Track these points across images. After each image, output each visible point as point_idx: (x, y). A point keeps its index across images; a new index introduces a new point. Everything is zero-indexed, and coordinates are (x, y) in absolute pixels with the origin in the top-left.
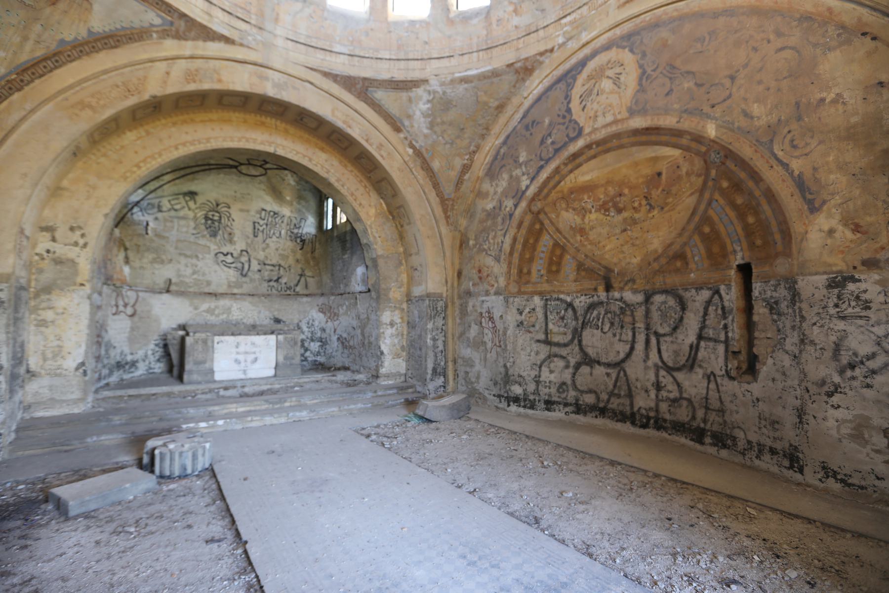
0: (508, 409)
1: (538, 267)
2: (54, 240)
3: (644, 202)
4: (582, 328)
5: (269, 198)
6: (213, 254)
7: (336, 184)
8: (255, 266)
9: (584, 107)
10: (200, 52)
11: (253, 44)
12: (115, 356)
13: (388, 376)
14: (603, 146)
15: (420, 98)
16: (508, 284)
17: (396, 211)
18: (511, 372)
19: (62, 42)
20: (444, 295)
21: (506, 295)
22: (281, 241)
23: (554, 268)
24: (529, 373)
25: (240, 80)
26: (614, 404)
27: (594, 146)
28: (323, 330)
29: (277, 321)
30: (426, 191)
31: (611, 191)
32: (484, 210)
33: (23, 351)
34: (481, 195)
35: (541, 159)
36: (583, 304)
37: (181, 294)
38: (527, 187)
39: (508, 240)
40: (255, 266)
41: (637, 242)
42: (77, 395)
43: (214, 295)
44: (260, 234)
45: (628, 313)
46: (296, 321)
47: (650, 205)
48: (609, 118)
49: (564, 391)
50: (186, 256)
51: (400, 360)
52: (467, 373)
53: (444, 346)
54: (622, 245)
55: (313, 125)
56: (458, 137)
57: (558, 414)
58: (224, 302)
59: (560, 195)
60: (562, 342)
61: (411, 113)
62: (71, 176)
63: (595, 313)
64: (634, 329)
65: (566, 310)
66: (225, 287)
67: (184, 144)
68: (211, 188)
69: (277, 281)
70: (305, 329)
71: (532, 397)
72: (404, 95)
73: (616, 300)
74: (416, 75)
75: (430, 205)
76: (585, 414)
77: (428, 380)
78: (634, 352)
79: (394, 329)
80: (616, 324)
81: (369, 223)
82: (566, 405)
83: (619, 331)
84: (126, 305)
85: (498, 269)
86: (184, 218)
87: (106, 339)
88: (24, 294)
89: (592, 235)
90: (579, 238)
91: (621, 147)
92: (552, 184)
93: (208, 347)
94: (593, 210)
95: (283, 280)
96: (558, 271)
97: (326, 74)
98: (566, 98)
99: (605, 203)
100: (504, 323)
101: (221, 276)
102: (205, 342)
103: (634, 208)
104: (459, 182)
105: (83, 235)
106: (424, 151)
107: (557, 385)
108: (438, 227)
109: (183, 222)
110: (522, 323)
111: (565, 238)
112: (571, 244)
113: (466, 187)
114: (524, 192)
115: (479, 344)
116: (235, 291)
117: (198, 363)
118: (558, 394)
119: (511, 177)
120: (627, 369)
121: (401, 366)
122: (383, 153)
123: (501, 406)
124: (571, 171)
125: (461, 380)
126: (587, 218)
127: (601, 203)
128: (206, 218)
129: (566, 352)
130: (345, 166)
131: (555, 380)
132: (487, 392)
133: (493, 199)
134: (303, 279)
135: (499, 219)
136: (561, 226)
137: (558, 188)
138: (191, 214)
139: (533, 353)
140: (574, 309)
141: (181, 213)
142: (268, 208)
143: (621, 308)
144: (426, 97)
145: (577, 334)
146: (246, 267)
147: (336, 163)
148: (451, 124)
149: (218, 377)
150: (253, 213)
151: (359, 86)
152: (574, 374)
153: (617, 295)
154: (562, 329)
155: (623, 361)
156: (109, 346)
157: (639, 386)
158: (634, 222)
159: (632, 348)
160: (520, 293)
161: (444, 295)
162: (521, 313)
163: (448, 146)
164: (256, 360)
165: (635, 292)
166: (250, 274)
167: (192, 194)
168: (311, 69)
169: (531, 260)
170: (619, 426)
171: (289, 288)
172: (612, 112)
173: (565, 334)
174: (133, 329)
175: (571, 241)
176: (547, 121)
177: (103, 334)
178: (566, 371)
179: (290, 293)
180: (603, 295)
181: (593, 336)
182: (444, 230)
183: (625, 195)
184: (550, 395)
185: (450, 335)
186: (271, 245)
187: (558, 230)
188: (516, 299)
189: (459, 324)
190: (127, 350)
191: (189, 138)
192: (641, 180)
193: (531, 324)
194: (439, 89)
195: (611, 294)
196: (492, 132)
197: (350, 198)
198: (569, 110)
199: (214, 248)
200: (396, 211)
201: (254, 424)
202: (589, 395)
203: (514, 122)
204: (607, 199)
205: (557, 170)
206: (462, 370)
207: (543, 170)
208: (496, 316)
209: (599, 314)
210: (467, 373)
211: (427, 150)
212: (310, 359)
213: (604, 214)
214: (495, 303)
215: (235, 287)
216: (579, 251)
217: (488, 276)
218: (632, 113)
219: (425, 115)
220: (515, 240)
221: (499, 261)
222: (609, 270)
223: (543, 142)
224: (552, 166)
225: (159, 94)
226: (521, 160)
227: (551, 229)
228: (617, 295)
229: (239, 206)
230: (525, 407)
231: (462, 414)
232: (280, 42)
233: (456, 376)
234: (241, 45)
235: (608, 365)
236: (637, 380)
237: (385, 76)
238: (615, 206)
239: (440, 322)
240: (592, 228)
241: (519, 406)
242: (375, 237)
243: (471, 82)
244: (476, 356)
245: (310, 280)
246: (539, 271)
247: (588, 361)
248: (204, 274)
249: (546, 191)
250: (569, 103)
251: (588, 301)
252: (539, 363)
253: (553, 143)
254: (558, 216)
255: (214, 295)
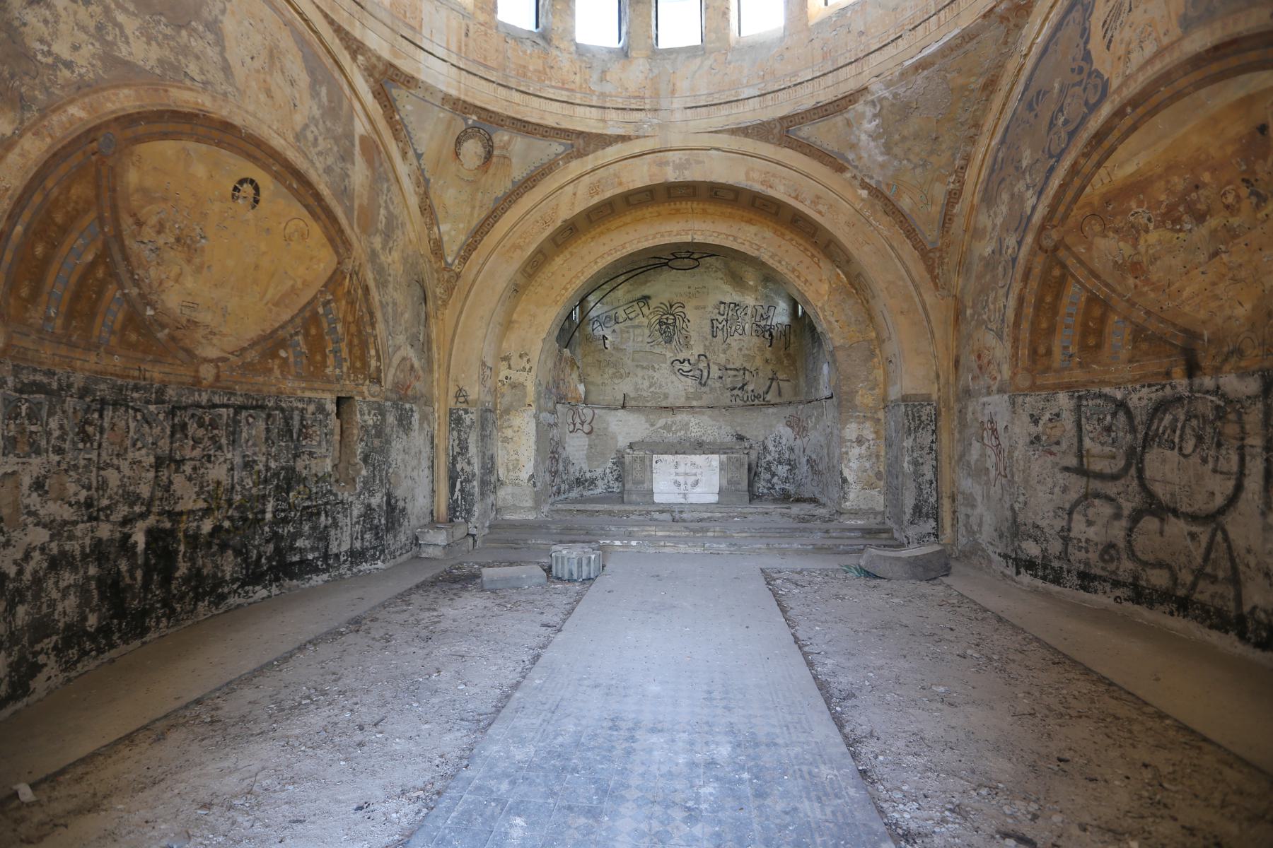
0: (1017, 579)
1: (1064, 342)
2: (510, 368)
3: (1244, 192)
4: (1144, 447)
5: (727, 288)
6: (669, 362)
7: (770, 262)
8: (715, 372)
9: (1110, 41)
10: (600, 162)
11: (649, 131)
12: (574, 472)
13: (856, 513)
14: (1144, 105)
15: (862, 115)
16: (1015, 374)
17: (856, 285)
18: (1021, 518)
19: (497, 198)
20: (935, 397)
21: (1013, 392)
22: (745, 338)
23: (1092, 341)
24: (1051, 524)
25: (639, 176)
26: (1205, 593)
27: (1129, 110)
28: (792, 449)
29: (740, 438)
30: (895, 244)
31: (1179, 183)
32: (982, 258)
33: (493, 463)
34: (977, 234)
35: (1051, 156)
36: (1144, 402)
37: (638, 409)
38: (1034, 208)
39: (1012, 302)
40: (715, 372)
41: (1243, 274)
42: (529, 503)
43: (672, 409)
44: (720, 333)
45: (1232, 417)
46: (761, 438)
47: (1258, 195)
48: (1150, 49)
49: (1112, 560)
50: (643, 368)
51: (875, 492)
52: (968, 516)
53: (935, 474)
54: (1214, 284)
55: (731, 196)
56: (931, 153)
57: (1102, 599)
58: (682, 417)
59: (1088, 211)
60: (1108, 471)
61: (853, 139)
62: (518, 309)
63: (1168, 418)
64: (1241, 449)
65: (1114, 415)
66: (683, 399)
67: (602, 257)
68: (663, 288)
69: (742, 388)
70: (772, 448)
71: (1056, 564)
72: (839, 120)
73: (1207, 392)
74: (852, 86)
75: (903, 264)
76: (1151, 605)
77: (905, 523)
78: (1243, 495)
79: (864, 447)
80: (1207, 440)
81: (820, 304)
82: (1116, 584)
83: (1212, 452)
84: (582, 423)
85: (1000, 350)
86: (638, 327)
87: (564, 455)
88: (489, 415)
89: (1156, 273)
90: (1131, 281)
91: (1177, 96)
92: (1070, 195)
93: (647, 468)
94: (1151, 226)
95: (750, 388)
96: (1098, 346)
97: (733, 132)
98: (1082, 37)
99: (1171, 208)
100: (1010, 438)
101: (678, 387)
102: (642, 460)
103: (1227, 207)
104: (946, 220)
105: (528, 361)
106: (884, 187)
107: (1100, 547)
108: (920, 294)
109: (638, 331)
110: (1038, 438)
111: (1107, 285)
112: (1119, 295)
113: (958, 226)
114: (1029, 218)
115: (979, 472)
116: (694, 403)
117: (636, 483)
118: (1101, 564)
119: (1012, 196)
120: (1229, 528)
121: (878, 500)
122: (820, 207)
123: (1007, 572)
124: (1099, 165)
125: (962, 530)
126: (1142, 241)
127: (1163, 210)
128: (661, 323)
129: (1115, 490)
130: (782, 235)
131: (1096, 539)
132: (991, 548)
133: (991, 238)
134: (774, 384)
135: (1000, 269)
136: (1097, 265)
137: (1082, 200)
138: (645, 321)
139: (1057, 489)
140: (1128, 413)
141: (636, 322)
142: (728, 300)
143: (1218, 407)
144: (869, 112)
145: (1135, 458)
146: (705, 374)
147: (769, 234)
148: (916, 136)
149: (657, 499)
150: (710, 309)
151: (776, 131)
152: (1131, 530)
153: (1208, 382)
154: (1107, 449)
155: (1222, 511)
156: (567, 462)
157: (1252, 564)
158: (1232, 233)
159: (1239, 488)
160: (1034, 388)
161: (935, 397)
162: (1036, 422)
163: (918, 171)
164: (697, 483)
165: (1243, 374)
166: (709, 382)
167: (646, 299)
168: (716, 132)
169: (1051, 331)
170: (1214, 637)
171: (757, 397)
172: (1154, 35)
173: (1114, 457)
174: (590, 446)
175: (1119, 288)
176: (1056, 85)
177: (560, 450)
178: (1116, 523)
179: (757, 402)
180: (1181, 383)
181: (1164, 461)
182: (929, 298)
183: (1205, 185)
184: (1087, 564)
185: (944, 458)
186: (734, 344)
187: (1093, 273)
188: (1028, 399)
189: (959, 441)
190: (586, 468)
191: (606, 249)
192: (1230, 150)
193: (1053, 440)
194: (886, 94)
195: (1197, 381)
196: (985, 129)
197: (790, 276)
198: (1087, 56)
199: (669, 354)
200: (856, 285)
201: (666, 550)
202: (1157, 572)
203: (1013, 103)
204: (1173, 199)
205: (1074, 170)
206: (962, 510)
207: (1054, 174)
208: (1000, 427)
209: (1176, 420)
210: (968, 516)
211: (888, 184)
212: (777, 487)
213: (1172, 229)
214: (998, 404)
215: (694, 399)
216: (1133, 305)
217: (989, 363)
218: (1187, 24)
219: (874, 137)
220: (1021, 300)
221: (1001, 338)
222: (1192, 335)
223: (1052, 124)
224: (1067, 163)
225: (568, 217)
226: (1024, 163)
227: (1081, 273)
228: (1208, 382)
229: (694, 302)
230: (1044, 578)
231: (933, 574)
232: (678, 116)
233: (955, 520)
234: (638, 137)
235: (1194, 518)
236: (1249, 551)
237: (808, 104)
238: (1191, 209)
239: (926, 438)
240: (1153, 260)
241: (1036, 576)
242: (830, 322)
243: (933, 64)
244: (977, 491)
245: (784, 385)
246: (1066, 348)
247: (1155, 507)
248: (661, 386)
249: (1062, 209)
250: (1087, 42)
251: (1153, 396)
252: (1067, 506)
253: (1066, 122)
254: (1089, 249)
255: (672, 409)
